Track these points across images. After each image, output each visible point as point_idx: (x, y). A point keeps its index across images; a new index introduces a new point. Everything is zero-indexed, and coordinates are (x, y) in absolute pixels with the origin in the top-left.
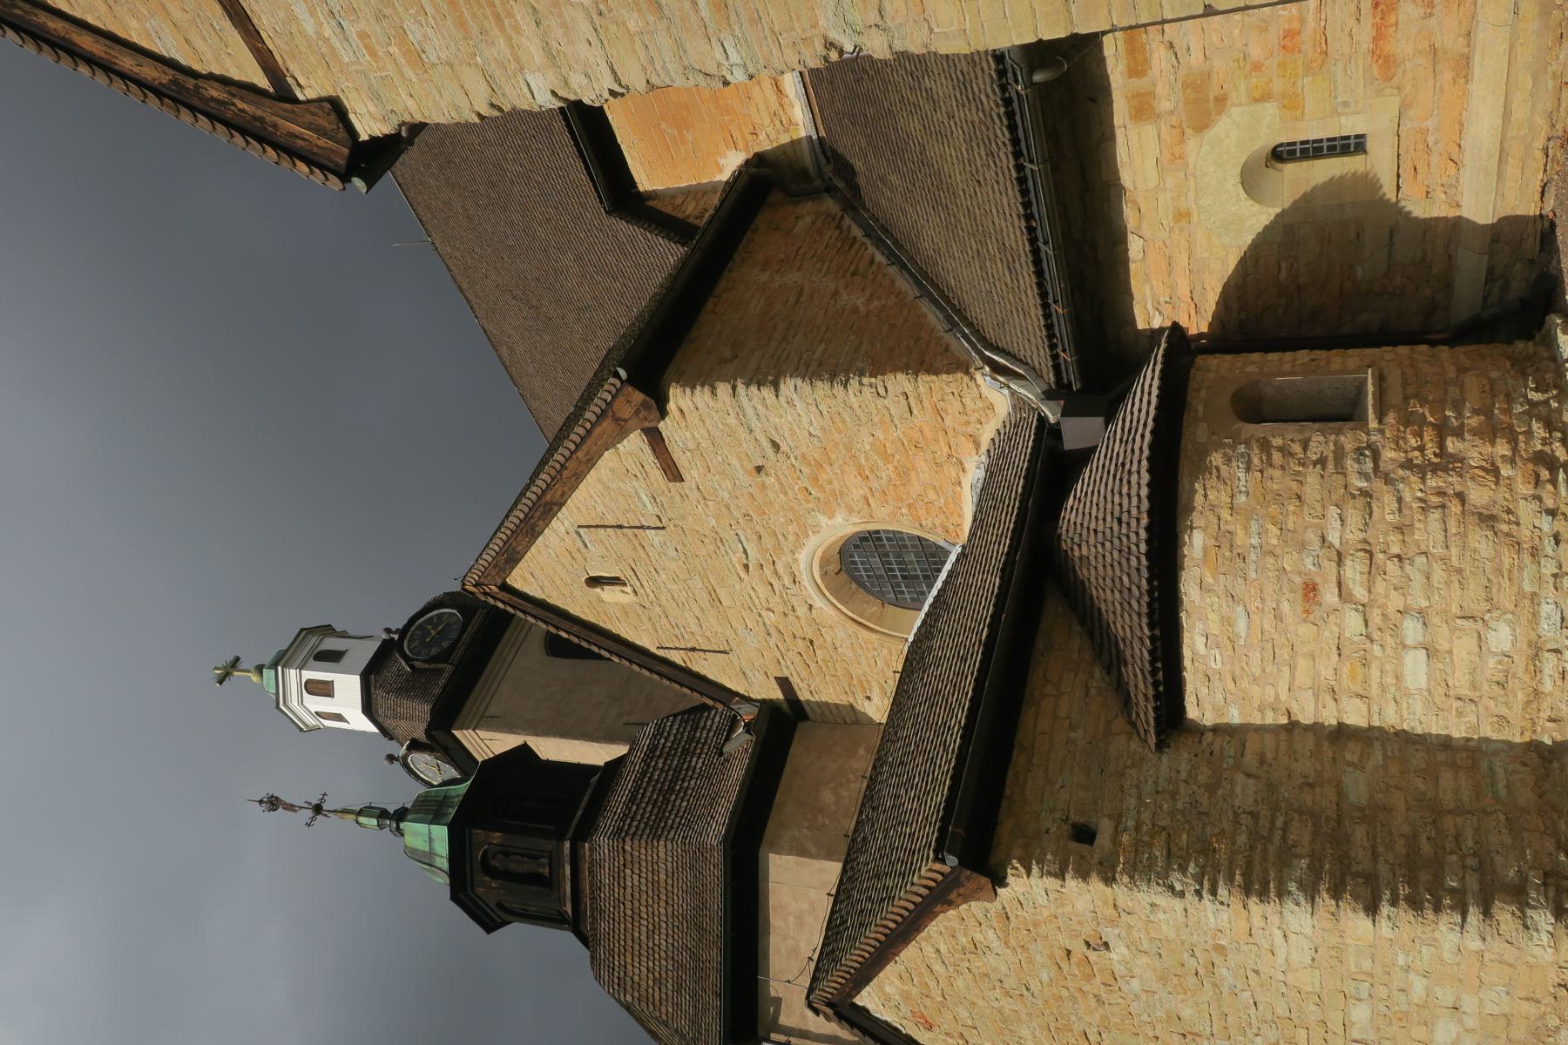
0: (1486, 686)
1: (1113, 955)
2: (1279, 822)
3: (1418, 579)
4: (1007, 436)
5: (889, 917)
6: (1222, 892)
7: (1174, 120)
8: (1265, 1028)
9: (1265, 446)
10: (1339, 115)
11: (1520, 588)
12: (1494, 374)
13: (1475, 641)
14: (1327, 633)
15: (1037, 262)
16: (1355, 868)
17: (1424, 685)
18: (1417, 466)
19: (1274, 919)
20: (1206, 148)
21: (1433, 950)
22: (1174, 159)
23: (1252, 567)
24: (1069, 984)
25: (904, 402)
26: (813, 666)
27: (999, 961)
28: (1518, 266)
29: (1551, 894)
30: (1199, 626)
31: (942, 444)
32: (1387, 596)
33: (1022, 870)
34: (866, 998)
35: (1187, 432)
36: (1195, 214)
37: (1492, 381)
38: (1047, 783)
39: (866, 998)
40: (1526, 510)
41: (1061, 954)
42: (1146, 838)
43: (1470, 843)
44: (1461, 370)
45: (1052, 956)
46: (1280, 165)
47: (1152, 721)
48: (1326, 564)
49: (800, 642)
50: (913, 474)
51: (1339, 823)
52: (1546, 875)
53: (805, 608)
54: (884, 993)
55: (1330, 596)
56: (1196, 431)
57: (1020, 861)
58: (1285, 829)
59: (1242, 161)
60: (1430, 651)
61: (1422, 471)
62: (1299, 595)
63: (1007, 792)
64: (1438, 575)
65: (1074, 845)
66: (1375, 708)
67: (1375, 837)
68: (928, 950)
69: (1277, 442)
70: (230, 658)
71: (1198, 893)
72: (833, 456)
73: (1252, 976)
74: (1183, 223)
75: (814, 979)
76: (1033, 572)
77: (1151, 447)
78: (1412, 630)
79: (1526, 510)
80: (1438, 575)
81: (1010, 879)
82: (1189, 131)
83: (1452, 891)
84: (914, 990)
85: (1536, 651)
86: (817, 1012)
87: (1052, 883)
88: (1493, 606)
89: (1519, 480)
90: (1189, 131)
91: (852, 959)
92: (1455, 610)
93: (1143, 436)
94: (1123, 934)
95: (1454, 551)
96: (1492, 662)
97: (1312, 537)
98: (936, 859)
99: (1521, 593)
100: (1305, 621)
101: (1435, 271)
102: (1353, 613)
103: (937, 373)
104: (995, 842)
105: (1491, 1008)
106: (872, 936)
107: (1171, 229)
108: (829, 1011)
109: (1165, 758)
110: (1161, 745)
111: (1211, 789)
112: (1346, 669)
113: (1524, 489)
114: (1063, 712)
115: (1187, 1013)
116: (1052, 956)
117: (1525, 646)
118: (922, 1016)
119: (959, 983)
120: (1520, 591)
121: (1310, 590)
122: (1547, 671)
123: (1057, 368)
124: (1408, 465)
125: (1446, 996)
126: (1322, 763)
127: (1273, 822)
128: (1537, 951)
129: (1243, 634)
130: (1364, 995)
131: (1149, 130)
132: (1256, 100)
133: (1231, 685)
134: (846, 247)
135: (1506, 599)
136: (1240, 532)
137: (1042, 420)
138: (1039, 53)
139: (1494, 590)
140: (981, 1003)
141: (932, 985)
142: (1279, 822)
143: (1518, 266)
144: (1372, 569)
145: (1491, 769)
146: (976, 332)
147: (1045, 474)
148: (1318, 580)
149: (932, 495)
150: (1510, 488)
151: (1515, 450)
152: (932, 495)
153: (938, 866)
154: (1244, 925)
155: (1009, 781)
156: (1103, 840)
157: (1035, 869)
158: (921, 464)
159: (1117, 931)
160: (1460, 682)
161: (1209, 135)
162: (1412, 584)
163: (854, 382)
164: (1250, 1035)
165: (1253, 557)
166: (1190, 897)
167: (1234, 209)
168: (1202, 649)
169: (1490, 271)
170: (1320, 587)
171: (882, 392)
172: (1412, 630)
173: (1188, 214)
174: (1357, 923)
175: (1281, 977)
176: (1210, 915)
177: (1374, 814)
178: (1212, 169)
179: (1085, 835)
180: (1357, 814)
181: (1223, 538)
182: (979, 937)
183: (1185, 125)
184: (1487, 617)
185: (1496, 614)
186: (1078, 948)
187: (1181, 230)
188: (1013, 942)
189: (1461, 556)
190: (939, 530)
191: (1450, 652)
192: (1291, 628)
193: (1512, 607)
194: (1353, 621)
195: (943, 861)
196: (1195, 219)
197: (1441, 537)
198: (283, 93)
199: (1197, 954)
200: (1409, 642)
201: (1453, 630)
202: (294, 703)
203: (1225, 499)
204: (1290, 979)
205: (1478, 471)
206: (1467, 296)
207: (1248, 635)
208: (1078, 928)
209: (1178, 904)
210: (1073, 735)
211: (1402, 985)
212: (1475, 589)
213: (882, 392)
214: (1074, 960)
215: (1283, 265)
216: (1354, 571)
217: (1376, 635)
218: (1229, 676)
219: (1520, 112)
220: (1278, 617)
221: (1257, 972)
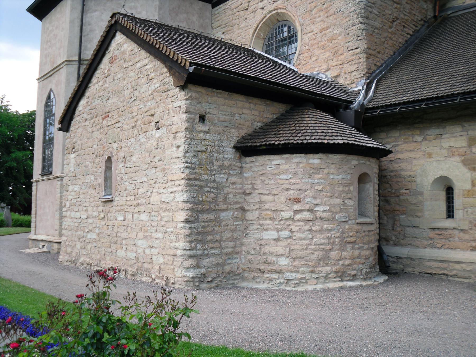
0: (265, 257)
1: (154, 131)
2: (212, 190)
3: (303, 236)
4: (343, 89)
5: (161, 44)
6: (188, 171)
7: (468, 152)
8: (133, 186)
9: (349, 185)
10: (464, 210)
11: (301, 267)
12: (371, 259)
13: (281, 253)
14: (282, 206)
15: (418, 101)
16: (200, 215)
17: (264, 238)
18: (342, 235)
19: (180, 188)
20: (456, 164)
21: (175, 240)
22: (452, 152)
23: (307, 181)
24: (139, 117)
25: (355, 47)
26: (236, 10)
27: (146, 89)
28: (402, 266)
29: (199, 276)
30: (283, 162)
31: (336, 63)
32: (296, 226)
33: (187, 97)
34: (119, 38)
35: (355, 157)
36: (430, 160)
37: (368, 259)
39: (119, 38)
40: (327, 269)
41: (152, 112)
42: (203, 143)
43: (212, 252)
44: (372, 248)
45: (150, 109)
46: (445, 190)
47: (246, 145)
48: (308, 206)
49: (247, 4)
50: (323, 51)
51: (214, 210)
52: (204, 274)
53: (262, 6)
54: (123, 44)
55: (297, 207)
56: (354, 161)
57: (191, 96)
58: (210, 192)
59: (449, 177)
60: (276, 240)
62: (296, 197)
63: (215, 90)
64: (306, 242)
65: (198, 116)
66: (254, 222)
67: (211, 222)
68: (146, 61)
69: (352, 188)
71: (186, 162)
72: (331, 18)
73: (154, 181)
74: (427, 156)
75: (125, 15)
76: (296, 99)
77: (353, 144)
78: (285, 233)
79: (327, 269)
80: (306, 242)
81: (183, 93)
82: (463, 158)
83: (196, 246)
84: (127, 56)
85: (280, 272)
86: (112, 17)
87: (184, 109)
88: (295, 259)
89: (338, 267)
90: (463, 158)
91: (140, 31)
92: (293, 247)
93: (319, 139)
94: (165, 135)
95: (313, 247)
96: (274, 259)
97: (318, 201)
98: (191, 63)
99: (299, 267)
100: (287, 198)
101: (402, 241)
102: (290, 215)
103: (366, 61)
104: (197, 86)
105: (154, 258)
106: (151, 38)
107: (425, 151)
108: (113, 22)
109: (231, 149)
111: (222, 166)
112: (269, 212)
113: (334, 268)
114: (245, 111)
115: (134, 159)
116: (150, 109)
117: (280, 269)
118: (115, 60)
119: (132, 74)
120: (299, 267)
121: (298, 201)
122: (272, 275)
123: (373, 108)
124: (343, 233)
125: (156, 243)
126: (232, 205)
127: (212, 188)
128: (179, 271)
129: (280, 177)
130: (152, 218)
131: (464, 144)
132: (472, 181)
133: (260, 173)
134: (414, 23)
135: (297, 263)
136: (319, 176)
137: (351, 102)
139: (300, 260)
140: (125, 82)
141: (131, 63)
142: (212, 190)
143: (402, 266)
144: (307, 221)
145: (235, 258)
146: (383, 76)
147: (333, 105)
148: (302, 203)
149: (314, 59)
150: (335, 265)
151: (348, 265)
152: (314, 59)
153: (188, 64)
154: (175, 178)
155: (218, 91)
156: (200, 127)
157: (188, 102)
158: (327, 54)
159: (165, 133)
160: (267, 249)
161: (461, 165)
162: (301, 234)
163: (362, 27)
164: (128, 181)
165: (310, 181)
166: (184, 160)
167: (431, 174)
168: (274, 163)
169: (401, 258)
170: (299, 204)
171: (360, 38)
172: (285, 233)
173: (430, 158)
174: (182, 216)
175: (155, 191)
176: (178, 166)
177: (217, 220)
178: (447, 166)
179: (202, 119)
180: (218, 216)
181: (317, 170)
182: (155, 81)
183: (466, 156)
184: (290, 257)
185: (291, 260)
186: (156, 119)
187: (424, 155)
188: (154, 94)
189: (312, 249)
190: (298, 62)
191: (277, 246)
192: (283, 194)
193: (294, 264)
194: (287, 215)
195: (190, 66)
196: (428, 160)
197: (318, 243)
199: (160, 162)
200: (280, 233)
201: (285, 247)
203: (331, 171)
204: (154, 194)
205: (340, 254)
206: (390, 250)
207: (280, 179)
208: (165, 118)
209: (181, 154)
210: (237, 115)
211: (158, 231)
212: (299, 253)
213: (360, 38)
214: (150, 117)
215: (408, 191)
216: (306, 215)
217: (282, 222)
218: (263, 172)
219: (458, 266)
220: (287, 190)
221: (155, 183)
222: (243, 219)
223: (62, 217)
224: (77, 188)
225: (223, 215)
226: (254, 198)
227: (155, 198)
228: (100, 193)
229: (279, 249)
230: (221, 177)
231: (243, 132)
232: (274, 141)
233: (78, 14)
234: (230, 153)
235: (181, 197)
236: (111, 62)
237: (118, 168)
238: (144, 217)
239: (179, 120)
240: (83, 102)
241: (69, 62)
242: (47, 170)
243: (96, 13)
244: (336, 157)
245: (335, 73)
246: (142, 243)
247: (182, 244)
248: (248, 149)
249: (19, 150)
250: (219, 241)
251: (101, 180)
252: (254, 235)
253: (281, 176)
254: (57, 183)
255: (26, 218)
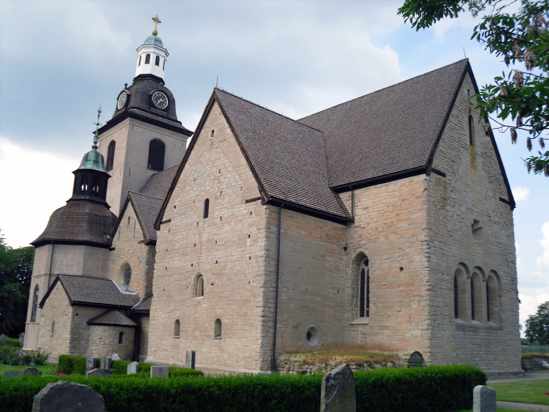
38: (82, 311)
56: (118, 328)
61: (112, 350)
70: (160, 20)
78: (97, 348)
110: (308, 340)
121: (101, 339)
138: (149, 314)
144: (103, 344)
156: (76, 317)
160: (93, 352)
172: (97, 348)
174: (68, 341)
179: (77, 315)
181: (107, 330)
194: (98, 342)
198: (161, 223)
202: (144, 50)
216: (103, 343)
222: (88, 343)
223: (38, 341)
224: (43, 330)
225: (81, 342)
226: (91, 337)
227: (64, 336)
228: (50, 333)
229: (95, 352)
230: (81, 331)
231: (90, 318)
232: (96, 322)
233: (50, 254)
234: (85, 324)
235: (69, 336)
236: (57, 289)
237: (56, 326)
238: (61, 341)
239: (70, 315)
240: (47, 300)
241: (46, 275)
242: (33, 320)
243: (58, 254)
244: (112, 327)
245: (137, 292)
246: (60, 349)
247: (68, 349)
248: (91, 323)
249: (11, 282)
250: (80, 349)
251: (51, 329)
252: (90, 348)
253: (98, 332)
254: (37, 326)
255: (359, 315)
